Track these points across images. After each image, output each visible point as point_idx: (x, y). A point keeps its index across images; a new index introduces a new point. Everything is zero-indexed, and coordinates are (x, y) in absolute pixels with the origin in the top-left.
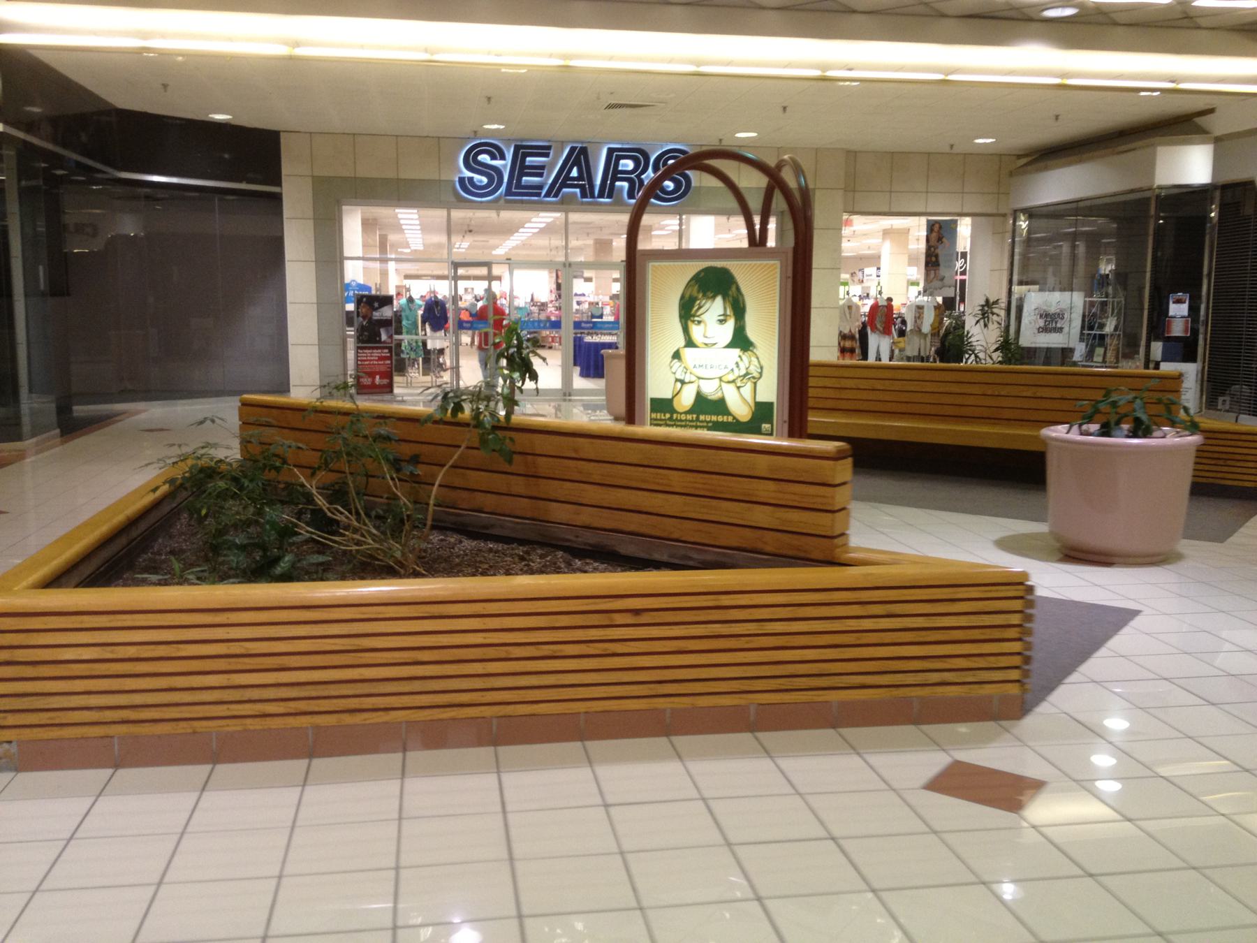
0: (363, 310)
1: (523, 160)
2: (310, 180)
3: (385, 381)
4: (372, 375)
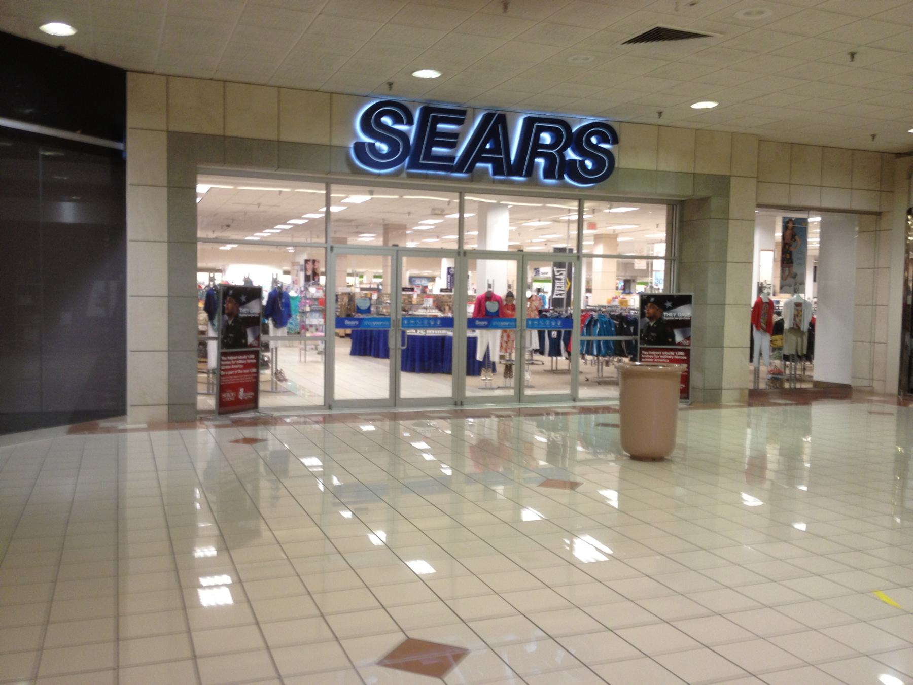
0: (650, 310)
1: (434, 127)
2: (164, 137)
3: (250, 395)
4: (235, 388)
